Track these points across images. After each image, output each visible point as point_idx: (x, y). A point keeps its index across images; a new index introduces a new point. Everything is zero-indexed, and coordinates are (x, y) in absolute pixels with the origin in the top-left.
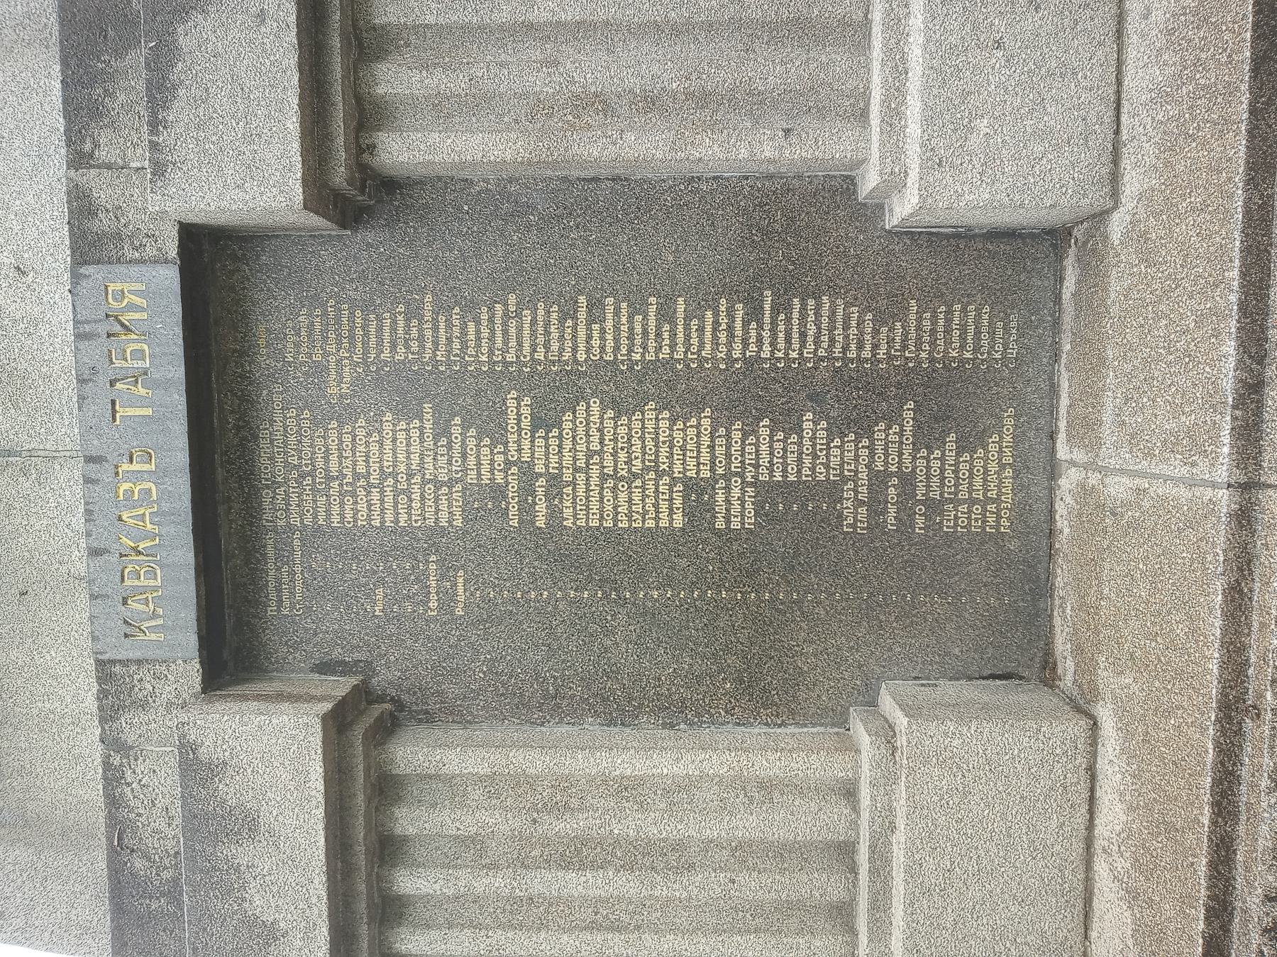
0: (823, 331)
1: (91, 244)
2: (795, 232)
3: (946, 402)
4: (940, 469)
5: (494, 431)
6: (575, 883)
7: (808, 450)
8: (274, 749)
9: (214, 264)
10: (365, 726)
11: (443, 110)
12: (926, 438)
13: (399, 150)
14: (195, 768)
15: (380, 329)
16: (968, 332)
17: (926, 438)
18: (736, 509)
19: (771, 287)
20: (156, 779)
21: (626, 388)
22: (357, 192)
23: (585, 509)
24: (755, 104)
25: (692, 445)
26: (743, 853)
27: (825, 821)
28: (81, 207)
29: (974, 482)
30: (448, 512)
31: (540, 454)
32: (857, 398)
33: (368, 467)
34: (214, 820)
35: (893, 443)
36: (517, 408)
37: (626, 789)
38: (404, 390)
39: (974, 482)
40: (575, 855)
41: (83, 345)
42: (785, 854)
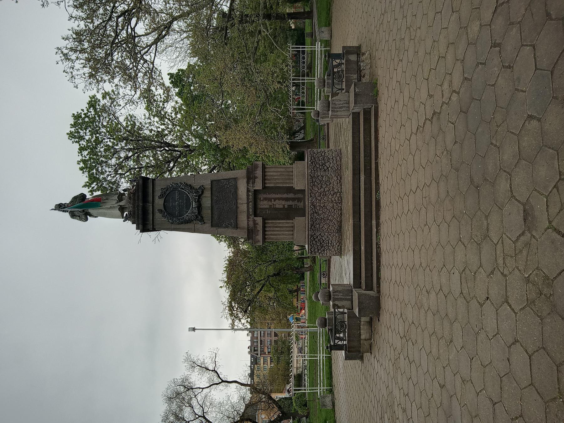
0: (291, 195)
1: (248, 191)
2: (290, 190)
3: (299, 200)
4: (299, 204)
5: (271, 201)
6: (276, 229)
7: (290, 203)
8: (259, 220)
9: (256, 192)
10: (264, 220)
11: (269, 183)
12: (298, 202)
13: (266, 185)
14: (254, 221)
15: (274, 235)
16: (300, 196)
17: (298, 202)
18: (286, 207)
19: (319, 399)
20: (251, 223)
21: (279, 199)
22: (264, 187)
23: (277, 206)
24: (287, 183)
25: (283, 202)
26: (287, 227)
27: (292, 225)
28: (248, 188)
29: (301, 205)
30: (268, 207)
31: (275, 203)
32: (293, 199)
33: (263, 204)
34: (255, 224)
35: (296, 202)
36: (273, 200)
37: (280, 223)
38: (265, 199)
39: (301, 205)
40: (277, 227)
41: (156, 227)
42: (289, 227)
